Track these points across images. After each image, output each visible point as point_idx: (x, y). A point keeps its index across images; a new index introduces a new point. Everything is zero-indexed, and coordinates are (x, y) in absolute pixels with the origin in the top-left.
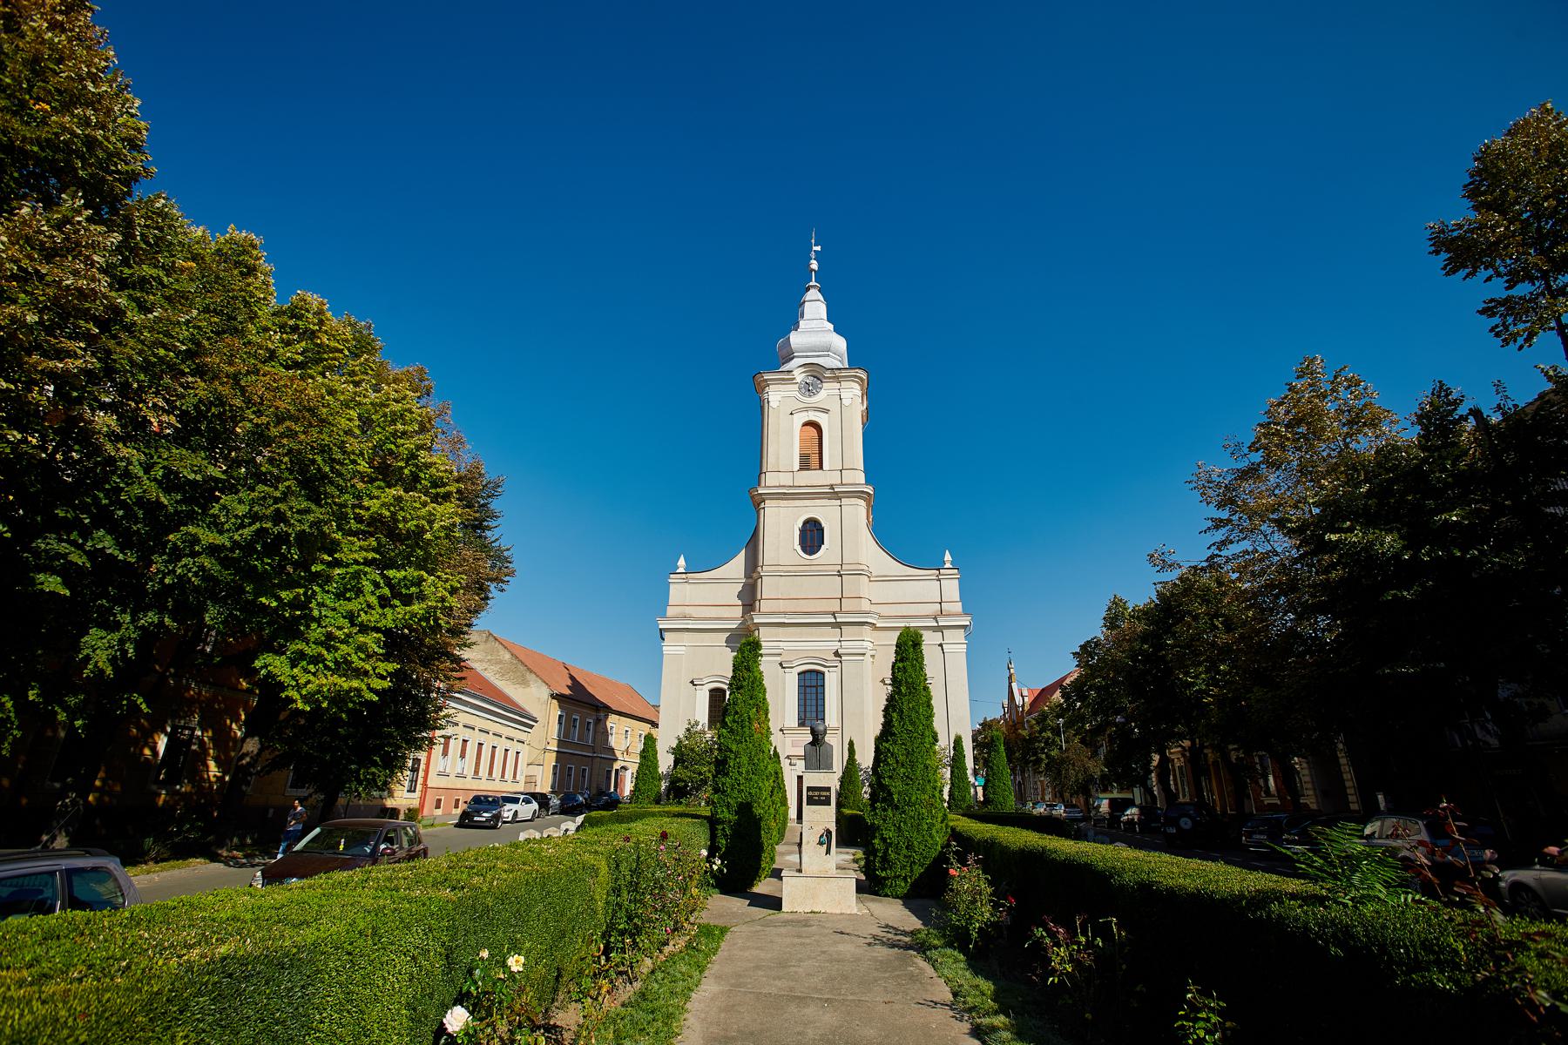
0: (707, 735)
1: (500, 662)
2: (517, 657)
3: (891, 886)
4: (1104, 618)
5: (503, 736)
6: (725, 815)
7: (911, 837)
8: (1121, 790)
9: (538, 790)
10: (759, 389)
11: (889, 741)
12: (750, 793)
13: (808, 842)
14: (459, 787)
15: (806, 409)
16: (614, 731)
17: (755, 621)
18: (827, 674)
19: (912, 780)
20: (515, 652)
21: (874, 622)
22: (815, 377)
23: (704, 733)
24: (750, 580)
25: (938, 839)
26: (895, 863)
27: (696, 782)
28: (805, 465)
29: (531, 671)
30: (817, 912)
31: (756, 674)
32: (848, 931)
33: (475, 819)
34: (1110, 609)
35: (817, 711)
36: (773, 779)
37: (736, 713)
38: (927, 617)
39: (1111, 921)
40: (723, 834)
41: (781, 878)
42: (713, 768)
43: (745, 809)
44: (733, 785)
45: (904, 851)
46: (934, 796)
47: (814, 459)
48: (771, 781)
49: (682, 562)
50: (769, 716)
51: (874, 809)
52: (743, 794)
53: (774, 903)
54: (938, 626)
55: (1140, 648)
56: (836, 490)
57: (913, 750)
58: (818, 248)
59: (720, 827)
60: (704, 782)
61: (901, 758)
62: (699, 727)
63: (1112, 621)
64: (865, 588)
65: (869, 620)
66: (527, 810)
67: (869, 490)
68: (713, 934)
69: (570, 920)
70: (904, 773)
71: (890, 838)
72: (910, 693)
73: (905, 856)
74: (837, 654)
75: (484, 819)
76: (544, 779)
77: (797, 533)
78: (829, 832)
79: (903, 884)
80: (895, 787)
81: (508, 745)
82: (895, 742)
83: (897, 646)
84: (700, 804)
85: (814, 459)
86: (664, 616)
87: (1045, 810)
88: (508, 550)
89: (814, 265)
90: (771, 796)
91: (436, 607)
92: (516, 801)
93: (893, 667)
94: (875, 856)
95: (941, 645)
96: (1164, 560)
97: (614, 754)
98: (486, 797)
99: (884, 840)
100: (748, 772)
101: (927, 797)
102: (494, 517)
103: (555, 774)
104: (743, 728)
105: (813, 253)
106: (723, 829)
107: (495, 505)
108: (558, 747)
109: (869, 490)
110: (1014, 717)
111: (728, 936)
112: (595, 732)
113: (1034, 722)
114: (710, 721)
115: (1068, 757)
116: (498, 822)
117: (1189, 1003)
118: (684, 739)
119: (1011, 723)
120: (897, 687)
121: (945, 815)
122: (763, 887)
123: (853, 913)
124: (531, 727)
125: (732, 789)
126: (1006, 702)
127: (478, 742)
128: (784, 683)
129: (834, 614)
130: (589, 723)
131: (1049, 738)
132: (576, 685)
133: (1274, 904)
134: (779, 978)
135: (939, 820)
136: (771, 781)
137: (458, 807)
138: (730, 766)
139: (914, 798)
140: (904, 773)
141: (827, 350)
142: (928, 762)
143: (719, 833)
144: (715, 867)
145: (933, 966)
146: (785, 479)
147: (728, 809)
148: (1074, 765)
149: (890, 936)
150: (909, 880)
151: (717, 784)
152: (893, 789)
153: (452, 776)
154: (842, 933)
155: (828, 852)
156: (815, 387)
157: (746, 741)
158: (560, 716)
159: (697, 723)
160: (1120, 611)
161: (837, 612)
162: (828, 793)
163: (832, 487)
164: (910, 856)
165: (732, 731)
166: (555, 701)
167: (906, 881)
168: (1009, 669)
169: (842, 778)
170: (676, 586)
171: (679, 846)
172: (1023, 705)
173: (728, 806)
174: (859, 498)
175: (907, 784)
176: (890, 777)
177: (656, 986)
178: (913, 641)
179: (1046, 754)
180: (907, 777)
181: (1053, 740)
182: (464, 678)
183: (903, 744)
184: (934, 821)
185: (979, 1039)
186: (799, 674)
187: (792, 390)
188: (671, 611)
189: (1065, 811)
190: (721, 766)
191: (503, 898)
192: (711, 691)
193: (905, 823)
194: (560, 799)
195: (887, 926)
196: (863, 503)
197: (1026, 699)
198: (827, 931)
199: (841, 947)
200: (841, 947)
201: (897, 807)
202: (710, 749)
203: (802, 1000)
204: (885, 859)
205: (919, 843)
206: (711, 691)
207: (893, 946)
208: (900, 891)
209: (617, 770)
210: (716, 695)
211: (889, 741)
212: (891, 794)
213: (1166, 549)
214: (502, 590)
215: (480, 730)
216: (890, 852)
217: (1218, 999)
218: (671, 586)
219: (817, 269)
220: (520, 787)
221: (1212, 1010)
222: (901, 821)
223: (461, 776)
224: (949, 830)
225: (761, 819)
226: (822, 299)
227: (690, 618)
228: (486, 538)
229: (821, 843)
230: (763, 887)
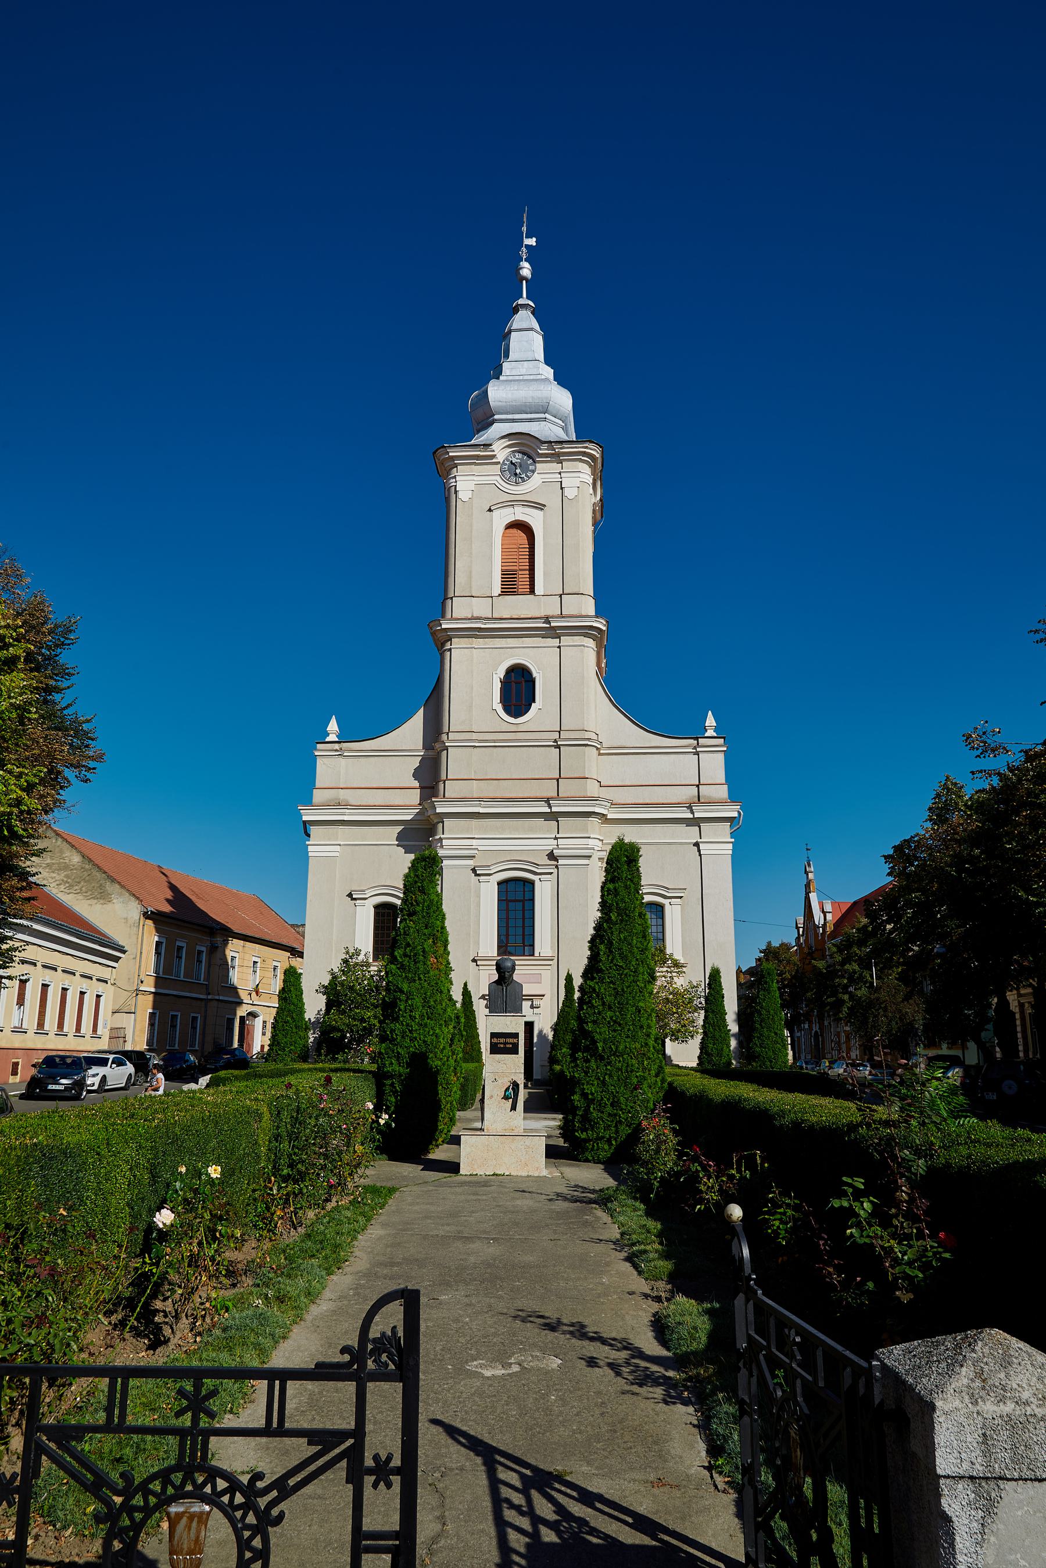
0: (372, 968)
1: (66, 867)
2: (90, 860)
3: (592, 1149)
4: (930, 809)
5: (77, 974)
6: (394, 1067)
7: (618, 1092)
8: (952, 1045)
9: (128, 1047)
10: (444, 470)
11: (595, 978)
12: (424, 1041)
13: (492, 1097)
14: (17, 1045)
15: (512, 504)
16: (237, 962)
17: (438, 810)
18: (537, 884)
19: (620, 1025)
20: (87, 853)
21: (605, 812)
22: (524, 453)
23: (368, 965)
24: (431, 753)
25: (650, 1095)
26: (598, 1123)
27: (358, 1031)
28: (509, 587)
29: (113, 880)
30: (500, 1175)
31: (433, 897)
32: (530, 1190)
33: (50, 1087)
34: (938, 796)
35: (523, 935)
36: (453, 1024)
37: (408, 945)
38: (677, 805)
39: (756, 1154)
40: (391, 1091)
41: (459, 1144)
42: (379, 1010)
43: (419, 1062)
44: (404, 1032)
45: (609, 1109)
46: (646, 1044)
47: (523, 577)
48: (451, 1027)
49: (333, 726)
50: (450, 948)
51: (574, 1059)
52: (416, 1043)
53: (453, 1167)
54: (694, 818)
55: (969, 854)
56: (552, 624)
57: (623, 990)
58: (532, 242)
59: (389, 1082)
60: (368, 1031)
61: (608, 999)
62: (361, 958)
63: (940, 813)
64: (594, 765)
65: (597, 810)
66: (119, 1074)
67: (601, 624)
68: (381, 1193)
69: (239, 1160)
70: (611, 1018)
71: (592, 1094)
72: (622, 921)
73: (610, 1115)
74: (551, 856)
75: (62, 1088)
76: (137, 1033)
77: (497, 686)
78: (515, 1085)
79: (606, 1147)
80: (600, 1033)
81: (100, 990)
82: (602, 980)
83: (607, 863)
84: (363, 1060)
85: (523, 577)
86: (308, 801)
87: (845, 1071)
88: (88, 721)
89: (526, 270)
90: (451, 1046)
91: (10, 814)
92: (103, 1062)
93: (602, 888)
94: (575, 1115)
95: (697, 844)
96: (985, 742)
97: (239, 997)
98: (63, 1058)
99: (584, 1095)
100: (422, 1016)
101: (638, 1045)
102: (65, 673)
103: (152, 1024)
104: (416, 963)
105: (524, 249)
106: (392, 1084)
107: (65, 657)
108: (155, 987)
109: (601, 624)
110: (812, 941)
111: (397, 1194)
112: (209, 965)
113: (834, 949)
114: (375, 949)
115: (878, 999)
116: (82, 1090)
117: (772, 1200)
118: (339, 974)
119: (806, 950)
120: (606, 914)
121: (661, 1067)
122: (440, 1153)
123: (541, 1175)
124: (116, 959)
125: (403, 1037)
126: (801, 920)
127: (41, 982)
128: (479, 897)
129: (547, 801)
130: (200, 952)
131: (854, 972)
132: (178, 898)
133: (862, 1128)
134: (448, 1225)
135: (653, 1073)
136: (451, 1027)
137: (16, 1074)
138: (400, 1010)
139: (621, 1047)
140: (611, 1018)
141: (543, 409)
142: (641, 1004)
143: (387, 1089)
144: (382, 1122)
145: (611, 1215)
146: (480, 608)
147: (398, 1060)
148: (885, 1009)
149: (576, 1193)
150: (614, 1142)
151: (385, 1032)
152: (597, 1037)
153: (7, 1031)
154: (524, 1191)
155: (514, 1108)
156: (525, 469)
157: (420, 979)
158: (158, 944)
159: (357, 952)
160: (952, 799)
161: (553, 798)
162: (515, 1041)
163: (547, 619)
164: (615, 1115)
165: (402, 967)
166: (150, 923)
167: (610, 1144)
168: (807, 873)
169: (556, 1024)
170: (325, 760)
171: (344, 1090)
172: (824, 926)
173: (398, 1056)
174: (586, 635)
175: (615, 1031)
176: (594, 1022)
177: (322, 1228)
178: (627, 857)
179: (850, 993)
180: (615, 1022)
181: (861, 975)
182: (33, 899)
183: (611, 982)
184: (646, 1075)
185: (630, 1262)
186: (499, 884)
187: (490, 474)
188: (318, 796)
189: (870, 1074)
190: (389, 1010)
191: (186, 1129)
192: (378, 908)
193: (611, 1076)
194: (162, 1060)
195: (576, 1186)
196: (591, 643)
197: (829, 917)
198: (507, 1190)
199: (518, 1202)
200: (518, 1202)
201: (602, 1058)
202: (377, 987)
203: (468, 1239)
204: (586, 1118)
205: (627, 1099)
206: (378, 908)
207: (576, 1201)
208: (602, 1155)
209: (242, 1018)
210: (384, 914)
211: (595, 978)
212: (594, 1042)
213: (988, 727)
214: (86, 781)
215: (44, 966)
216: (591, 1109)
217: (795, 1198)
218: (319, 761)
219: (529, 276)
220: (103, 1044)
221: (788, 1205)
222: (606, 1074)
223: (19, 1030)
224: (666, 1085)
225: (438, 1072)
226: (537, 326)
227: (346, 805)
228: (54, 703)
229: (506, 1098)
230: (440, 1153)
